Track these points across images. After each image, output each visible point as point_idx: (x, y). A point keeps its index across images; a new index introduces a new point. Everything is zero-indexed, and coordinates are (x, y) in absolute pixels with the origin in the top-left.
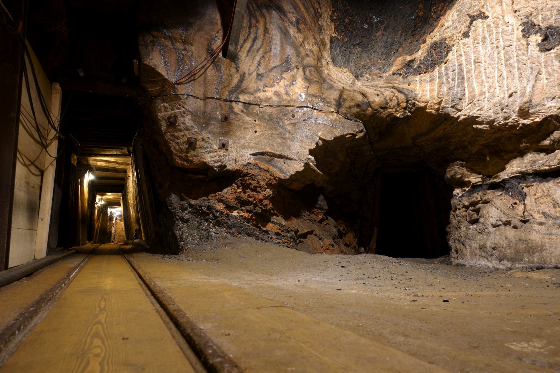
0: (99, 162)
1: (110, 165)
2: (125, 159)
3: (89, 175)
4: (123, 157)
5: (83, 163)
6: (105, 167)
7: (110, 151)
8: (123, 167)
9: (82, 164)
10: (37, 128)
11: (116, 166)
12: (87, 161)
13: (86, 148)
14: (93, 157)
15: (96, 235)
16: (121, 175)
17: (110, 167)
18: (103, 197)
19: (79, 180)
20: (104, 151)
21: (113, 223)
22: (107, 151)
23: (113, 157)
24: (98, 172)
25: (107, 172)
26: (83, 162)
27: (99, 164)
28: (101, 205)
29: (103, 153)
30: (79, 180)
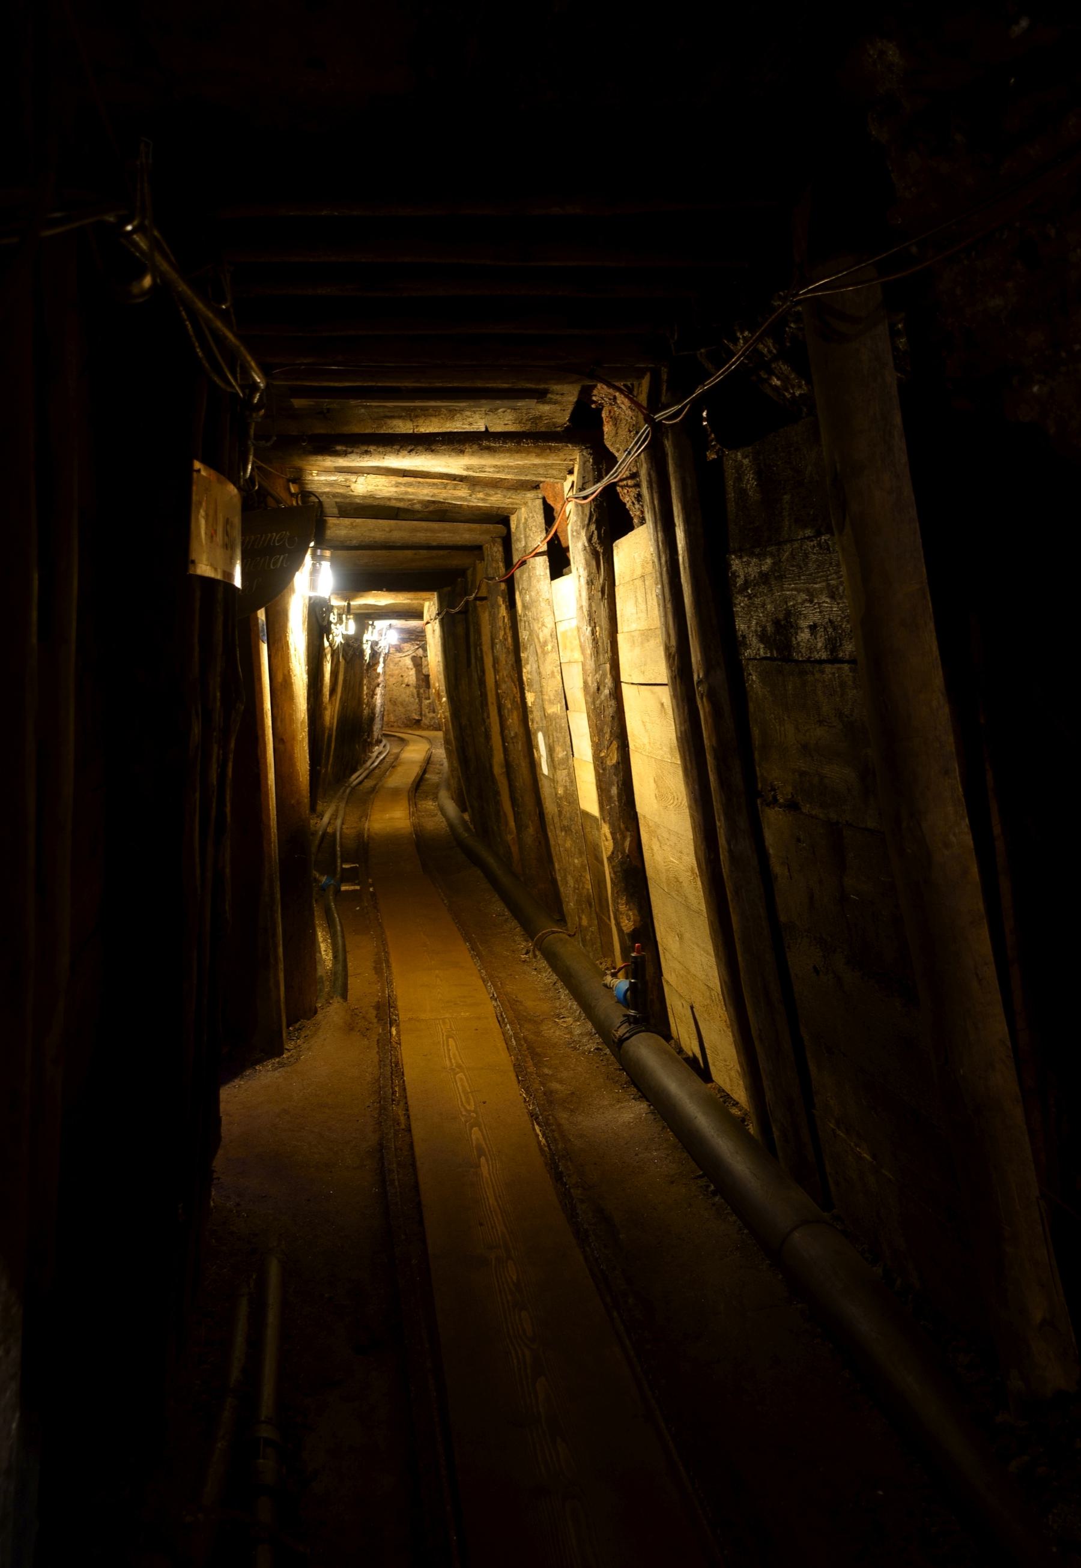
0: (361, 479)
1: (424, 492)
2: (537, 461)
3: (314, 571)
4: (528, 452)
5: (278, 501)
6: (393, 503)
7: (452, 414)
8: (496, 500)
9: (271, 503)
10: (626, 388)
11: (460, 495)
12: (298, 478)
13: (298, 403)
14: (337, 454)
15: (329, 746)
16: (467, 536)
17: (421, 502)
18: (352, 603)
19: (261, 614)
20: (411, 415)
21: (379, 674)
22: (426, 414)
23: (462, 452)
24: (347, 521)
25: (392, 522)
26: (279, 491)
27: (363, 486)
28: (345, 637)
29: (404, 427)
30: (261, 614)
